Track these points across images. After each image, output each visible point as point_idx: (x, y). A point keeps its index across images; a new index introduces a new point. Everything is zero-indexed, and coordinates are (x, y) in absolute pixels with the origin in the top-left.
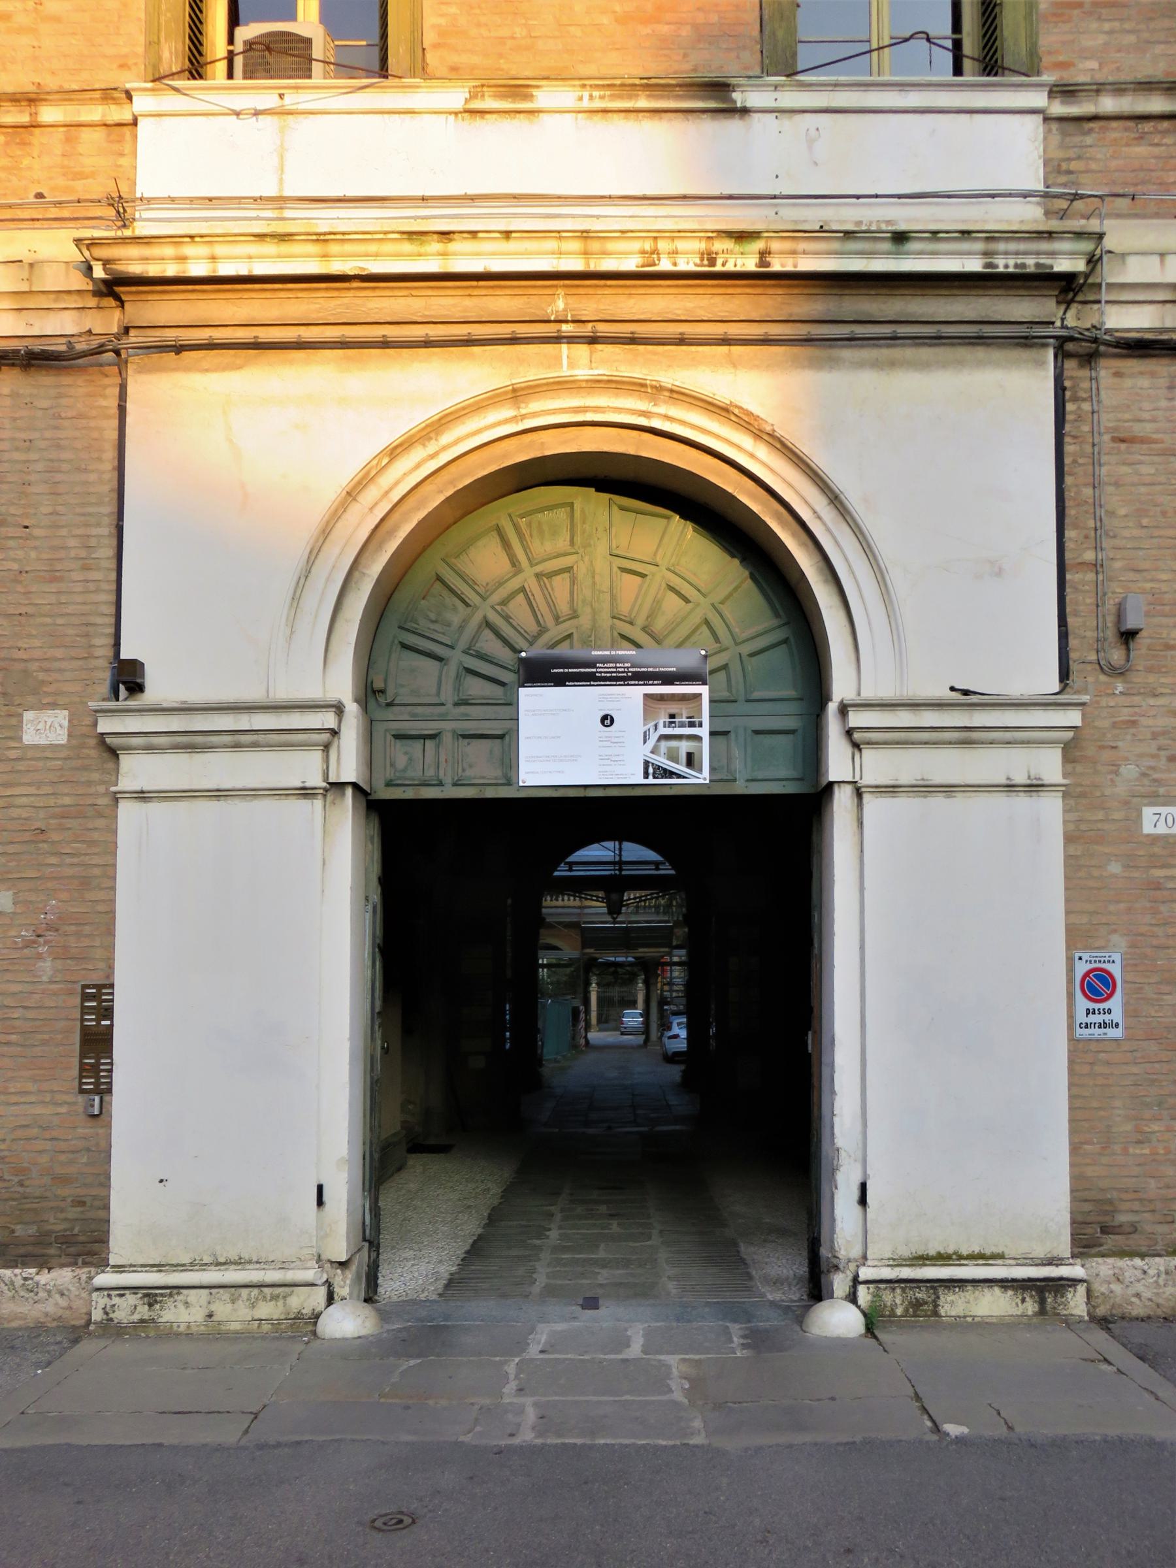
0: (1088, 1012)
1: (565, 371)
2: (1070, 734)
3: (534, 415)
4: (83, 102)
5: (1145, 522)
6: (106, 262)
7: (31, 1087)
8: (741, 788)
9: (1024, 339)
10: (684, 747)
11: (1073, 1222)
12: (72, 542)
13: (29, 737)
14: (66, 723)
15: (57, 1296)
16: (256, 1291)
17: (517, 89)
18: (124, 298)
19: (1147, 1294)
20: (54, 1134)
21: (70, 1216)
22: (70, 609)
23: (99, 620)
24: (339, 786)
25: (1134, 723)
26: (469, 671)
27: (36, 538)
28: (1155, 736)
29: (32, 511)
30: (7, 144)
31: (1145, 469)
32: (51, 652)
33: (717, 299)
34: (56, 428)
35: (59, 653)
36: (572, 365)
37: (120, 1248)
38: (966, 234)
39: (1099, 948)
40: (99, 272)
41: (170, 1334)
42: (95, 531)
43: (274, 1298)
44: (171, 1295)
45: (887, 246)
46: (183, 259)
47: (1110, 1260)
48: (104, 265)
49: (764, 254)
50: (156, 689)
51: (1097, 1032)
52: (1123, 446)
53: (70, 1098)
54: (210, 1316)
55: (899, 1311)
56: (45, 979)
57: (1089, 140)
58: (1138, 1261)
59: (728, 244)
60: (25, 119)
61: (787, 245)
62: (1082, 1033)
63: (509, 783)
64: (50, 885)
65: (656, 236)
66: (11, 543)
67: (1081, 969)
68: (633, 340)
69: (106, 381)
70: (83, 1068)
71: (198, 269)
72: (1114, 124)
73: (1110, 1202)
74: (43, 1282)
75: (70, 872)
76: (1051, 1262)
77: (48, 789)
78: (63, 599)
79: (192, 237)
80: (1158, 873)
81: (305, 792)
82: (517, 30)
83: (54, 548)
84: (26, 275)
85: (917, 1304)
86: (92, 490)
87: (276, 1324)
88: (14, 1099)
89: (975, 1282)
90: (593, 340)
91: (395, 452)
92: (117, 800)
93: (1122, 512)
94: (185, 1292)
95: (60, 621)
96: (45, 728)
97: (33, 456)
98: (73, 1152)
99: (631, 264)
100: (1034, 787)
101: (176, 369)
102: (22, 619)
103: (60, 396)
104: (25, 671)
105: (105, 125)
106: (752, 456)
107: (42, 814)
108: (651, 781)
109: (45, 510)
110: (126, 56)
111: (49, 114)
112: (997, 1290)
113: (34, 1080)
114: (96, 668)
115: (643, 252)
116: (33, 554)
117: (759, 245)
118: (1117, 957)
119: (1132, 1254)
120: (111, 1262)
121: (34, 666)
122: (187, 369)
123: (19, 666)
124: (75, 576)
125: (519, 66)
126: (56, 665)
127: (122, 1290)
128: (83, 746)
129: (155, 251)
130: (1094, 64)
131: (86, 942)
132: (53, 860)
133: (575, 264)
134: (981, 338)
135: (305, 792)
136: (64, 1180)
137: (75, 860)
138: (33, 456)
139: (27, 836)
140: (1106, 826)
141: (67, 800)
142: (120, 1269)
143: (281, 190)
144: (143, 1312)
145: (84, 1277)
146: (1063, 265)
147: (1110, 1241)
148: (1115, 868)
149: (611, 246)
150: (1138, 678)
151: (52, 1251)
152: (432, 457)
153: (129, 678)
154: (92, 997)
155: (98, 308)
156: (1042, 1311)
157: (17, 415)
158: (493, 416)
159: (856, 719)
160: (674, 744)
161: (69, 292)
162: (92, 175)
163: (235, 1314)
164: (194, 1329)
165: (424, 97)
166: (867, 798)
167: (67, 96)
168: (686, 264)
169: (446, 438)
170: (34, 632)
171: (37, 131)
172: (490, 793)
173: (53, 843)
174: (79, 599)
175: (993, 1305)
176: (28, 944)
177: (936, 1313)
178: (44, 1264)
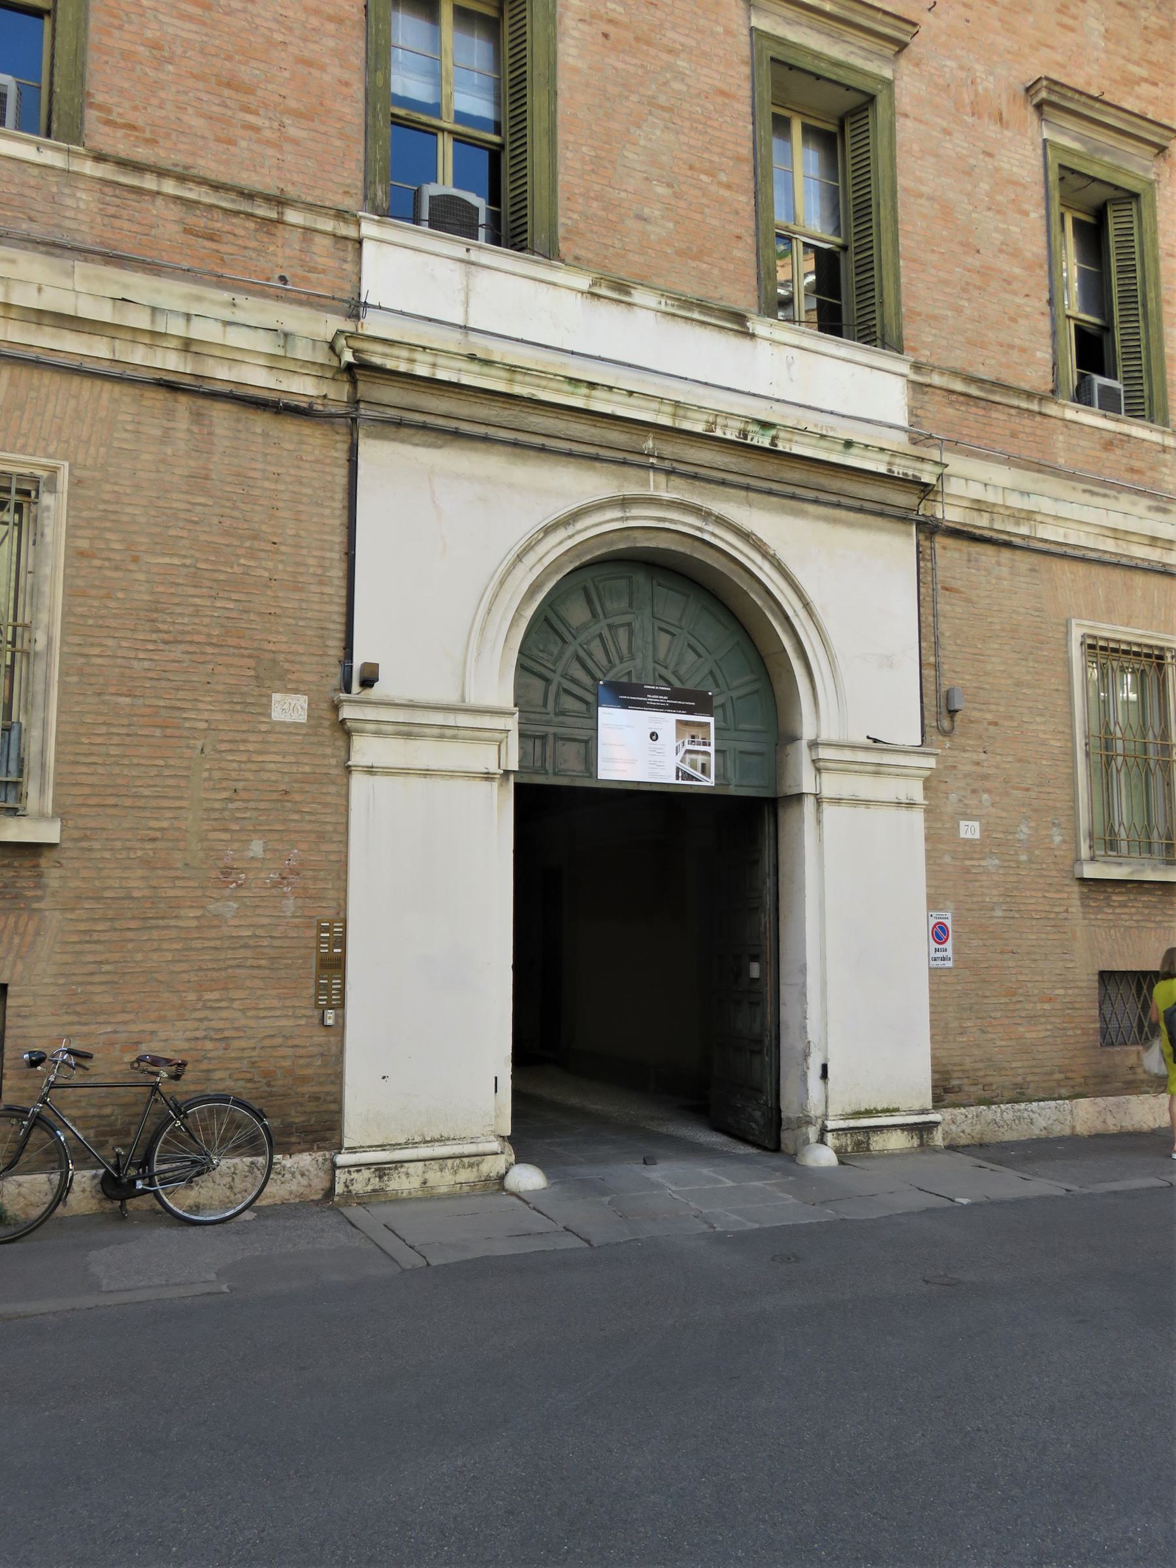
1: (651, 492)
2: (929, 773)
3: (634, 518)
4: (319, 214)
5: (958, 642)
6: (356, 352)
7: (276, 1003)
8: (732, 791)
9: (902, 518)
10: (700, 759)
11: (934, 1087)
12: (311, 561)
13: (277, 715)
14: (306, 706)
15: (299, 1177)
16: (458, 1161)
17: (622, 287)
18: (358, 377)
19: (968, 1131)
20: (296, 1042)
21: (308, 1109)
22: (310, 614)
23: (332, 626)
25: (955, 767)
26: (566, 691)
27: (283, 553)
29: (279, 531)
30: (256, 230)
32: (294, 648)
33: (740, 460)
34: (299, 467)
35: (301, 649)
36: (656, 487)
37: (353, 1131)
38: (882, 450)
39: (941, 910)
40: (348, 357)
41: (397, 1200)
42: (328, 555)
43: (471, 1165)
44: (396, 1168)
45: (840, 448)
46: (412, 361)
47: (949, 1110)
48: (353, 353)
49: (774, 438)
51: (940, 963)
52: (947, 593)
53: (309, 1012)
54: (425, 1183)
55: (849, 1149)
56: (289, 914)
57: (926, 398)
58: (962, 1110)
59: (756, 428)
60: (273, 215)
61: (788, 436)
62: (934, 964)
63: (590, 777)
64: (293, 836)
65: (718, 413)
66: (262, 555)
67: (933, 922)
68: (695, 477)
69: (338, 437)
70: (319, 986)
71: (422, 371)
72: (938, 392)
74: (289, 1165)
75: (309, 827)
76: (923, 1112)
77: (292, 759)
78: (304, 606)
79: (424, 348)
81: (488, 777)
82: (616, 242)
83: (297, 564)
84: (281, 342)
86: (326, 521)
87: (473, 1185)
88: (263, 1013)
90: (670, 473)
91: (548, 530)
92: (350, 772)
93: (947, 634)
94: (406, 1165)
95: (301, 623)
96: (290, 708)
97: (281, 487)
98: (310, 1057)
99: (699, 428)
100: (911, 805)
101: (394, 440)
102: (273, 619)
103: (301, 442)
104: (274, 661)
105: (334, 235)
106: (761, 568)
107: (286, 779)
108: (680, 782)
109: (291, 532)
110: (348, 186)
111: (293, 216)
113: (279, 997)
114: (329, 664)
115: (707, 422)
116: (281, 566)
117: (773, 432)
118: (949, 915)
120: (346, 1145)
121: (281, 657)
122: (403, 441)
123: (270, 656)
124: (314, 588)
125: (622, 273)
126: (298, 658)
127: (359, 1166)
128: (319, 725)
129: (396, 351)
131: (321, 885)
132: (296, 817)
133: (666, 421)
134: (882, 513)
135: (488, 777)
136: (305, 1080)
137: (313, 818)
138: (281, 487)
139: (275, 796)
140: (942, 832)
141: (307, 769)
142: (352, 1150)
143: (467, 319)
144: (375, 1183)
145: (320, 1159)
146: (926, 479)
147: (950, 1097)
148: (947, 859)
149: (690, 414)
151: (294, 1139)
152: (570, 537)
154: (326, 930)
155: (333, 379)
156: (921, 1145)
157: (268, 451)
159: (824, 753)
160: (694, 756)
161: (314, 363)
162: (324, 272)
163: (443, 1180)
164: (414, 1194)
165: (561, 276)
166: (825, 806)
167: (310, 207)
168: (731, 435)
169: (580, 525)
170: (281, 630)
171: (281, 226)
173: (295, 802)
174: (316, 607)
175: (897, 1142)
176: (275, 885)
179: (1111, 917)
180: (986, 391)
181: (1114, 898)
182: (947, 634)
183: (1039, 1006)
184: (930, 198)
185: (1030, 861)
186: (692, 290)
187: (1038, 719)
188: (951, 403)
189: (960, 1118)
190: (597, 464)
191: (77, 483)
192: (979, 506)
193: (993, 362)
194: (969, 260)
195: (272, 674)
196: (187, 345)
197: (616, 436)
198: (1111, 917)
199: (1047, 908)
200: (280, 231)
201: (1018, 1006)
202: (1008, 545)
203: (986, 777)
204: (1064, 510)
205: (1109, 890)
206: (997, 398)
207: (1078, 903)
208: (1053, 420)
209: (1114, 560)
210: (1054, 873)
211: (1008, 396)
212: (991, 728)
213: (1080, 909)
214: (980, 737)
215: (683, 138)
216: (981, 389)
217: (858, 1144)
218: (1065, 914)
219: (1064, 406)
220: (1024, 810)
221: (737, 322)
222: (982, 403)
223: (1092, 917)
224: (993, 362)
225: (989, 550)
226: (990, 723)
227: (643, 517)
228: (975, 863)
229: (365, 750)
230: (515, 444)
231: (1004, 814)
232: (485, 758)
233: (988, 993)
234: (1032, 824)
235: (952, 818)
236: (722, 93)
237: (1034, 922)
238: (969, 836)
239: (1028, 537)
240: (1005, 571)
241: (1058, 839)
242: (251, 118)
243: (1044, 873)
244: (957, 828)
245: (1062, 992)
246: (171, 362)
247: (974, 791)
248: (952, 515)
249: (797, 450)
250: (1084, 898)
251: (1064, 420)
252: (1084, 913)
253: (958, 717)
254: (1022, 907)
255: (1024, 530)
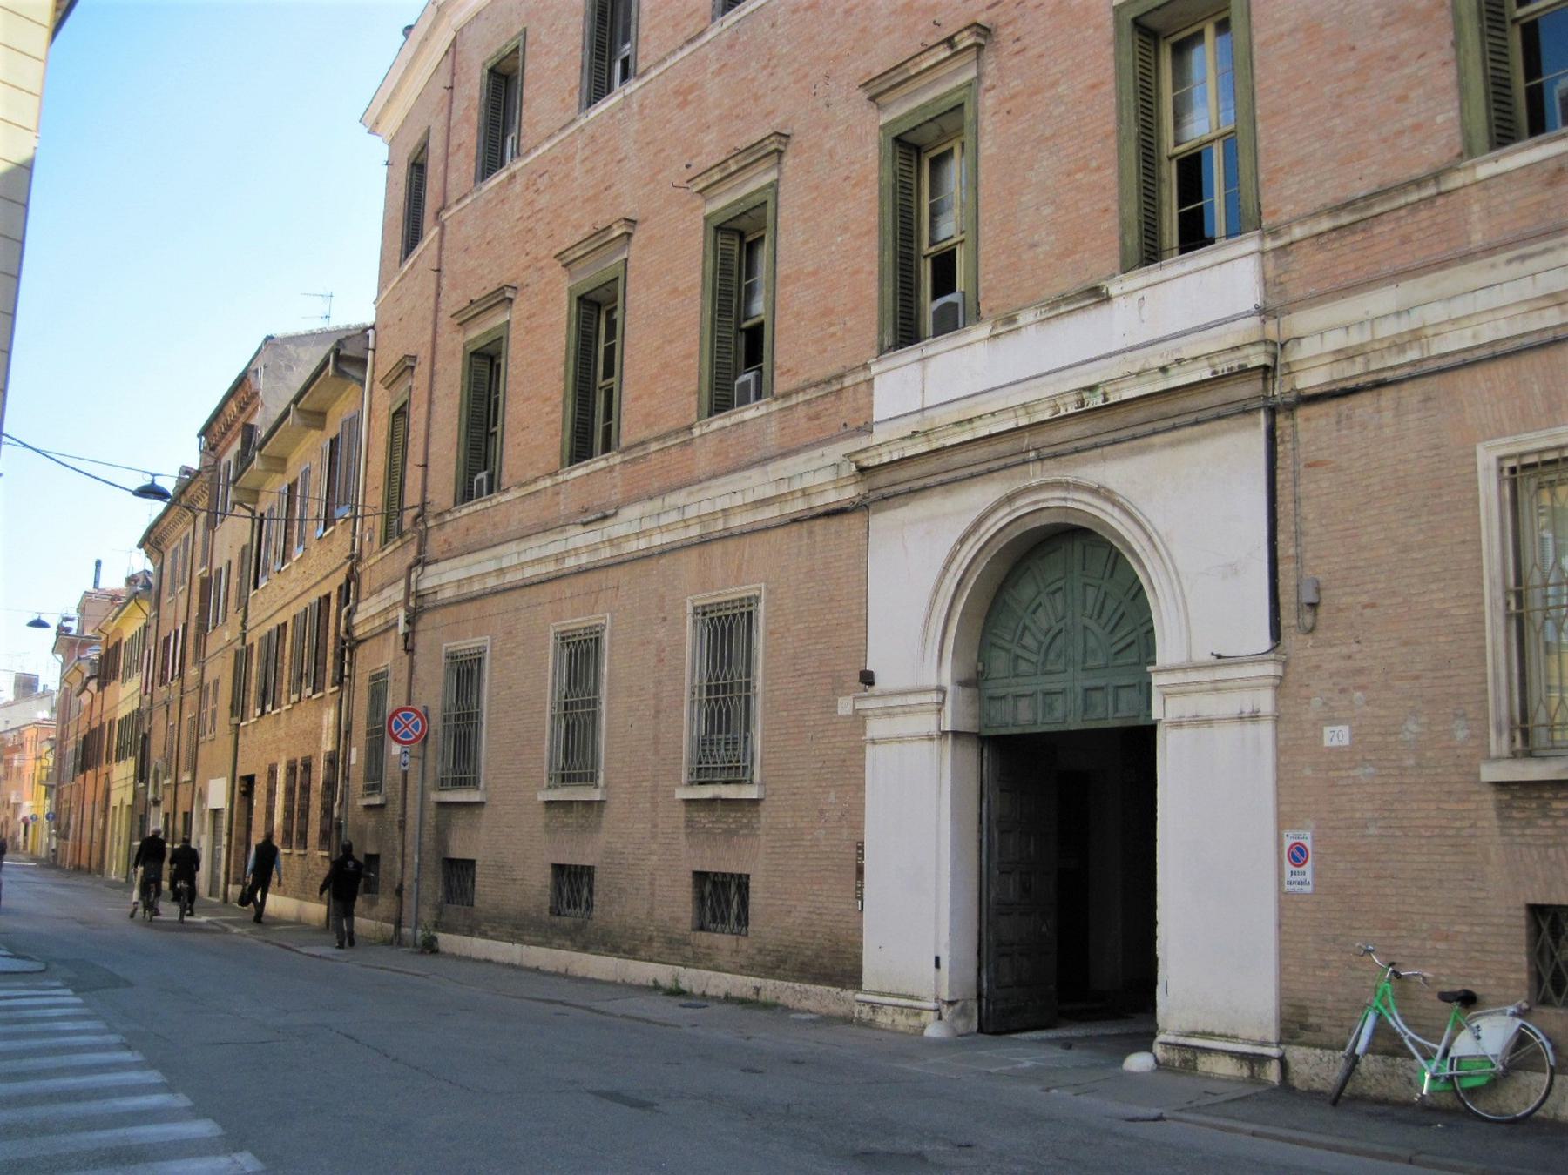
0: (1292, 873)
13: (841, 711)
17: (1011, 320)
24: (945, 733)
25: (1318, 667)
28: (1331, 675)
31: (1324, 484)
45: (1160, 375)
50: (881, 683)
51: (1296, 887)
58: (1318, 1051)
62: (1287, 888)
65: (1053, 398)
67: (1288, 843)
71: (886, 459)
73: (1304, 1007)
80: (1332, 774)
81: (930, 738)
85: (1185, 1061)
89: (1216, 1051)
91: (962, 541)
99: (1047, 416)
100: (1255, 717)
111: (848, 382)
112: (1228, 1058)
117: (1100, 391)
118: (1308, 834)
119: (1315, 1046)
130: (1290, 207)
133: (1023, 422)
134: (1220, 415)
135: (930, 738)
142: (866, 992)
147: (1307, 1036)
148: (1308, 772)
150: (1321, 635)
153: (867, 679)
156: (1252, 1075)
158: (1002, 513)
169: (983, 530)
172: (1028, 731)
175: (1225, 1067)
177: (1195, 1068)
178: (844, 987)
179: (1549, 832)
180: (1361, 210)
181: (1555, 805)
182: (1311, 517)
183: (1429, 944)
184: (1294, 30)
185: (1419, 765)
186: (1050, 293)
187: (1433, 587)
188: (1322, 248)
189: (1311, 1059)
190: (928, 492)
191: (770, 592)
192: (1345, 355)
193: (1374, 168)
194: (1341, 67)
195: (838, 688)
196: (805, 493)
197: (1004, 447)
198: (1549, 832)
199: (1443, 822)
200: (845, 394)
201: (1399, 942)
202: (1379, 385)
203: (1360, 671)
204: (1459, 308)
205: (1547, 795)
206: (1377, 210)
207: (1492, 814)
208: (1462, 192)
209: (1458, 359)
210: (1455, 778)
211: (1392, 198)
212: (1368, 612)
213: (1496, 823)
214: (1352, 626)
215: (1063, 153)
216: (1353, 211)
217: (1185, 1061)
218: (1471, 831)
219: (1473, 166)
220: (1411, 703)
221: (1097, 295)
222: (1360, 226)
223: (1516, 832)
224: (1374, 168)
225: (1366, 399)
226: (1365, 607)
227: (1024, 505)
228: (1344, 774)
229: (875, 728)
230: (942, 484)
231: (1382, 713)
232: (928, 723)
233: (1356, 924)
234: (1424, 719)
235: (1314, 724)
236: (1093, 87)
237: (1423, 841)
238: (1335, 743)
239: (1420, 361)
240: (1388, 416)
241: (1461, 735)
242: (832, 330)
243: (1440, 779)
244: (1319, 737)
245: (1465, 929)
246: (798, 506)
247: (1342, 691)
248: (1310, 380)
249: (1126, 395)
250: (1503, 810)
251: (1477, 183)
252: (1502, 828)
253: (1322, 610)
254: (1406, 823)
255: (1413, 355)
